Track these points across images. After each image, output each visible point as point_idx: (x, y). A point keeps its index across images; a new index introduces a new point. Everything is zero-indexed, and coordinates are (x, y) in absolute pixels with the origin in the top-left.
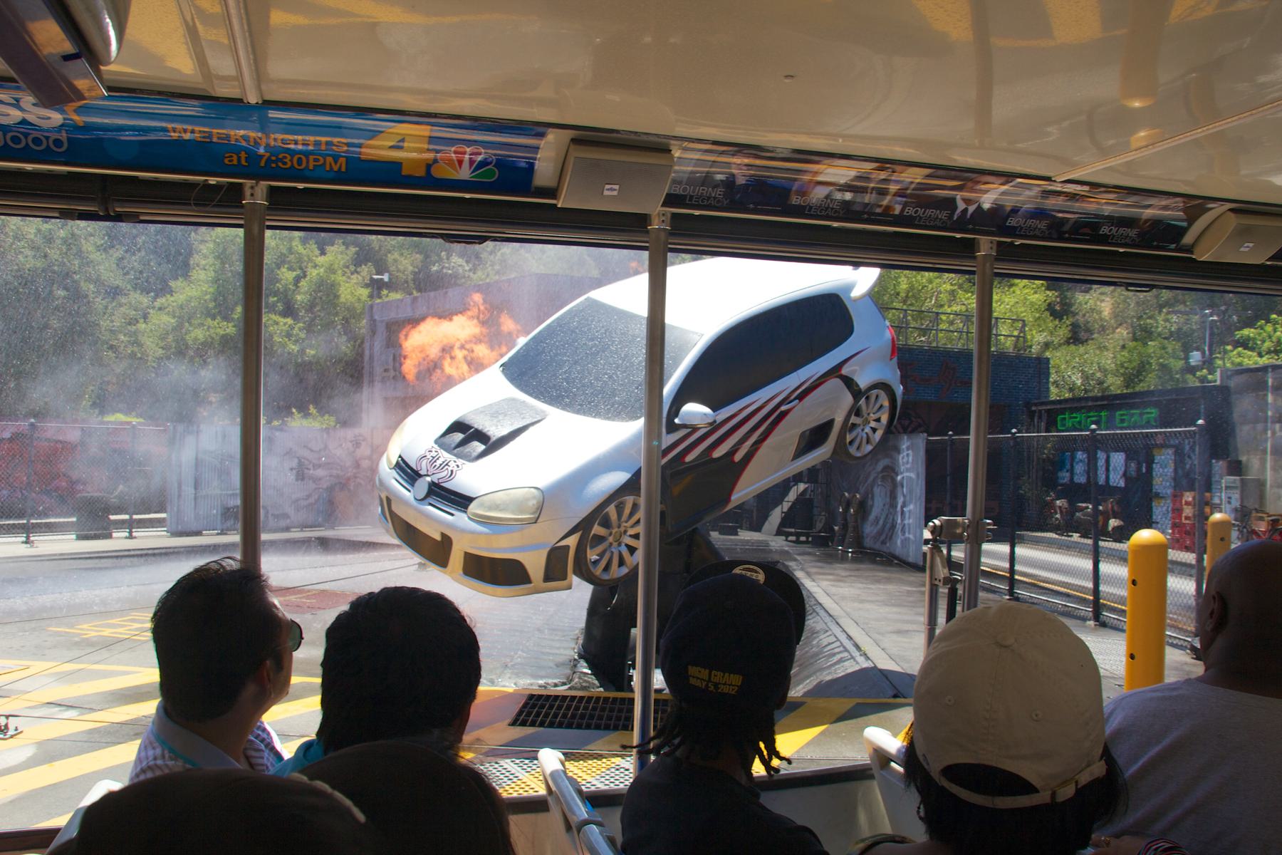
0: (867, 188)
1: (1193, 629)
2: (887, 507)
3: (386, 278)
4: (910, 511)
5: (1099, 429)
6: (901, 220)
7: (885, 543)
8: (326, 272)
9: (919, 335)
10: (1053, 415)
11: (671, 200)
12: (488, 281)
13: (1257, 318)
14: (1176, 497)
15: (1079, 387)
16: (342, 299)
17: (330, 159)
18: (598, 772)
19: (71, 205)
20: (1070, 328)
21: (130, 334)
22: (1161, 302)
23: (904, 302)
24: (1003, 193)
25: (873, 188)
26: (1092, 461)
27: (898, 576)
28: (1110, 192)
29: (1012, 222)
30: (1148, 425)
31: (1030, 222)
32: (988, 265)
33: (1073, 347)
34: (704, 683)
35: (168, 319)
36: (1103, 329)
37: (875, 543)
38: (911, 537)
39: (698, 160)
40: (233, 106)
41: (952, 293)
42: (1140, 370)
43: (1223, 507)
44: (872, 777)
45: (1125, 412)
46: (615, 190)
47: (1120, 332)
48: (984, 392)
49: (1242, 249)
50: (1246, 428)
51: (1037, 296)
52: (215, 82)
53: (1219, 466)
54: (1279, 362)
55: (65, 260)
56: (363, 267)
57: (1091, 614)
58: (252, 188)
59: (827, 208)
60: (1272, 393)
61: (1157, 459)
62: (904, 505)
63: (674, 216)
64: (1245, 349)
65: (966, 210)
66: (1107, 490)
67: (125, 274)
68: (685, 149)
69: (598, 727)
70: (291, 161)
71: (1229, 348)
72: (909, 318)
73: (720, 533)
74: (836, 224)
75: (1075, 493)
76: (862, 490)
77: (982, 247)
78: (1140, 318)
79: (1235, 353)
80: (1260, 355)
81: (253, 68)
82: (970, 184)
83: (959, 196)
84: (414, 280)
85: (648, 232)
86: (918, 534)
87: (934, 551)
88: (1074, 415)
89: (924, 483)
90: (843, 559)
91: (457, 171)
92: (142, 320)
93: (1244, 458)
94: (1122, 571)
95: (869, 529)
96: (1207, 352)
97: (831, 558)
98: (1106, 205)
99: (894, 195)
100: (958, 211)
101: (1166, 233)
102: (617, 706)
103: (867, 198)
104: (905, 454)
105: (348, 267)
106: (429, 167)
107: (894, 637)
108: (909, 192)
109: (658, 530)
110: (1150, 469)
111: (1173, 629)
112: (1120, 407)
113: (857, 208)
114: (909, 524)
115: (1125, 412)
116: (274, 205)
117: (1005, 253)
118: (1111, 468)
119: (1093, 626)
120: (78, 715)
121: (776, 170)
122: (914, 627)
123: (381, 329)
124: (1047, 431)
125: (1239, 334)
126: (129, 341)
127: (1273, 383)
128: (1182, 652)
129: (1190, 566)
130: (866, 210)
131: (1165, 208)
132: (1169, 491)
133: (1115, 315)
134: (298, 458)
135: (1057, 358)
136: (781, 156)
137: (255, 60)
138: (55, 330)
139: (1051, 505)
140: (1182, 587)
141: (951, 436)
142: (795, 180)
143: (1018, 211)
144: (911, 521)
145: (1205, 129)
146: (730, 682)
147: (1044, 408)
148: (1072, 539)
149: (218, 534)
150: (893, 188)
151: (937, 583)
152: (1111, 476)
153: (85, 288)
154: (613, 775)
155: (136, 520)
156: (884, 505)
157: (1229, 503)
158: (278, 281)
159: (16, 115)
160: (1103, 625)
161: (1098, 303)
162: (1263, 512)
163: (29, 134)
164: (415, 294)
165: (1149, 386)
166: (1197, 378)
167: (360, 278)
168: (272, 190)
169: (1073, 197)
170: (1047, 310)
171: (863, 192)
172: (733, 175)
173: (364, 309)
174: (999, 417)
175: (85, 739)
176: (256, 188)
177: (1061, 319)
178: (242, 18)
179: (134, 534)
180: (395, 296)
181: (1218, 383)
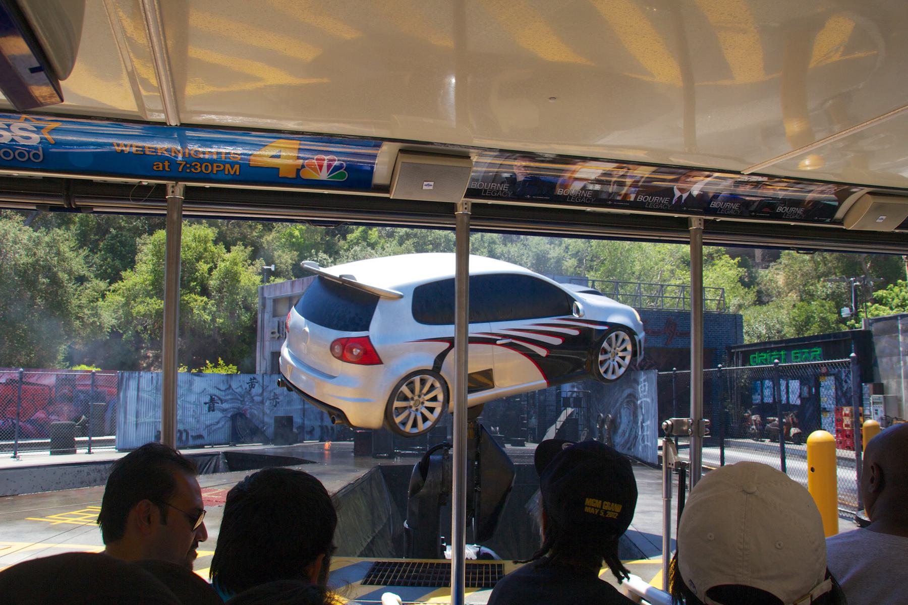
0: (610, 181)
2: (631, 423)
3: (273, 268)
4: (647, 426)
5: (781, 362)
7: (631, 449)
8: (231, 264)
10: (747, 354)
11: (471, 193)
13: (888, 283)
14: (838, 411)
15: (764, 336)
16: (242, 284)
17: (228, 166)
19: (44, 200)
20: (755, 294)
21: (93, 308)
22: (818, 274)
23: (639, 278)
24: (707, 184)
25: (615, 182)
26: (777, 385)
28: (783, 182)
29: (714, 205)
30: (815, 359)
31: (727, 204)
32: (698, 236)
33: (758, 307)
37: (623, 449)
38: (649, 444)
39: (490, 163)
40: (159, 129)
41: (672, 272)
42: (808, 321)
45: (798, 351)
46: (431, 185)
47: (790, 296)
48: (699, 327)
49: (878, 221)
50: (885, 360)
51: (732, 272)
52: (147, 112)
53: (867, 388)
54: (905, 313)
55: (48, 257)
58: (173, 187)
60: (902, 335)
61: (822, 384)
62: (643, 422)
63: (474, 205)
64: (880, 305)
65: (681, 196)
66: (788, 407)
67: (90, 267)
69: (426, 585)
70: (201, 167)
71: (869, 304)
72: (642, 290)
73: (512, 445)
75: (765, 410)
76: (612, 412)
77: (693, 224)
78: (805, 285)
79: (873, 307)
80: (891, 309)
81: (173, 98)
82: (683, 178)
83: (676, 187)
84: (292, 269)
86: (654, 441)
87: (668, 443)
89: (657, 405)
91: (319, 174)
93: (884, 382)
94: (804, 466)
96: (854, 308)
98: (779, 191)
99: (630, 186)
101: (823, 210)
102: (439, 570)
103: (611, 189)
104: (642, 385)
105: (246, 261)
106: (298, 171)
109: (466, 434)
111: (842, 506)
112: (794, 348)
113: (604, 196)
114: (647, 435)
115: (798, 351)
117: (710, 228)
118: (790, 390)
121: (546, 170)
122: (654, 508)
123: (269, 305)
124: (743, 365)
125: (875, 294)
126: (91, 314)
128: (851, 522)
129: (852, 460)
130: (610, 198)
131: (822, 192)
133: (787, 284)
134: (210, 395)
135: (748, 315)
137: (175, 93)
138: (40, 306)
139: (746, 420)
140: (848, 475)
141: (675, 371)
142: (560, 176)
143: (719, 196)
145: (847, 131)
147: (740, 350)
150: (629, 181)
151: (670, 466)
152: (790, 396)
156: (629, 422)
157: (876, 413)
158: (197, 271)
161: (775, 276)
165: (814, 333)
167: (255, 268)
168: (187, 190)
169: (757, 184)
170: (739, 281)
171: (608, 185)
172: (515, 174)
173: (257, 290)
174: (710, 357)
177: (749, 288)
178: (165, 61)
179: (92, 451)
180: (279, 281)
181: (863, 328)
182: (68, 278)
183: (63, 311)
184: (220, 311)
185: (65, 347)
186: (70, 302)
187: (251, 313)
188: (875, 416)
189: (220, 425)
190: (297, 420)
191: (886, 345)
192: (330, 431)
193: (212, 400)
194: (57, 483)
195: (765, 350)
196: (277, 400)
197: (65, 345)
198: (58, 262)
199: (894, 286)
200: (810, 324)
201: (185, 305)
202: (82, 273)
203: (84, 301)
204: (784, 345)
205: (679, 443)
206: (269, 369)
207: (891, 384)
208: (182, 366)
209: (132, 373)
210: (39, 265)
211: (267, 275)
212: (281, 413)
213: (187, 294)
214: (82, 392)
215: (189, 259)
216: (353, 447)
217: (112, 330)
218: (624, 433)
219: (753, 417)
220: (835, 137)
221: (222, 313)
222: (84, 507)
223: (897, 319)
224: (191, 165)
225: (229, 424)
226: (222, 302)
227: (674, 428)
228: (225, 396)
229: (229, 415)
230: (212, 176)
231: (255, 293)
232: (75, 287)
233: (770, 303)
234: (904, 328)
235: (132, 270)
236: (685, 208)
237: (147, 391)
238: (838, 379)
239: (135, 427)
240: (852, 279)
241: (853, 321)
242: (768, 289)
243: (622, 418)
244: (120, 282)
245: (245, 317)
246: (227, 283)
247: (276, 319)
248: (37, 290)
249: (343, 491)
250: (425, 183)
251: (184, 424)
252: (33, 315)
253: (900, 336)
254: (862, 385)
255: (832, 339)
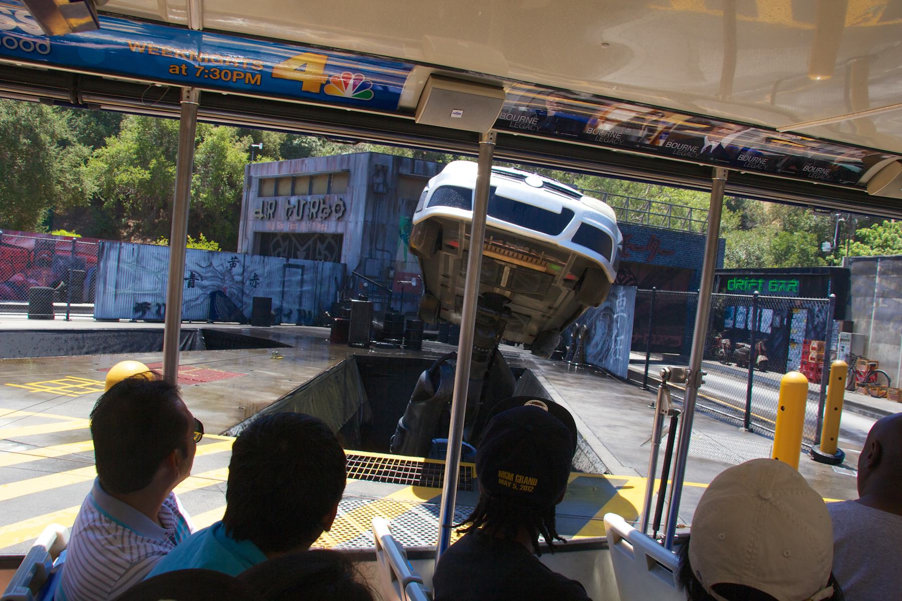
1: (814, 440)
2: (605, 336)
3: (260, 146)
4: (621, 340)
6: (663, 151)
7: (602, 361)
9: (635, 216)
11: (499, 124)
12: (333, 153)
14: (806, 344)
16: (229, 160)
17: (249, 75)
18: (396, 515)
20: (740, 218)
21: (75, 174)
23: (626, 191)
27: (609, 385)
29: (742, 158)
31: (754, 159)
32: (721, 187)
33: (741, 232)
34: (510, 484)
35: (103, 165)
36: (763, 221)
38: (621, 358)
39: (522, 96)
42: (788, 251)
43: (838, 353)
44: (607, 548)
45: (776, 282)
50: (858, 299)
53: (838, 324)
56: (245, 137)
57: (743, 423)
58: (188, 92)
59: (611, 138)
60: (879, 276)
62: (617, 336)
63: (498, 134)
64: (861, 243)
68: (514, 88)
70: (220, 74)
74: (615, 150)
75: (737, 335)
76: (588, 322)
77: (717, 174)
80: (872, 248)
85: (479, 145)
88: (740, 281)
90: (572, 370)
91: (343, 91)
92: (83, 164)
93: (855, 320)
94: (774, 396)
95: (591, 350)
96: (835, 243)
97: (562, 369)
100: (705, 147)
104: (621, 300)
105: (234, 137)
106: (322, 86)
107: (606, 429)
108: (671, 130)
110: (789, 323)
112: (772, 277)
115: (776, 282)
116: (204, 105)
117: (733, 179)
118: (762, 319)
119: (744, 431)
120: (27, 450)
125: (859, 231)
127: (880, 270)
128: (805, 454)
129: (815, 393)
130: (639, 141)
132: (802, 339)
136: (583, 98)
138: (20, 167)
139: (717, 342)
142: (591, 116)
144: (621, 347)
146: (529, 483)
147: (719, 274)
148: (730, 367)
149: (130, 322)
150: (660, 128)
151: (663, 413)
152: (762, 325)
153: (43, 138)
154: (406, 518)
155: (66, 302)
156: (603, 334)
157: (842, 350)
159: (11, 24)
160: (751, 431)
162: (865, 359)
163: (21, 39)
164: (281, 160)
165: (792, 264)
166: (827, 261)
167: (242, 145)
168: (203, 94)
171: (638, 129)
175: (31, 468)
176: (191, 92)
177: (734, 211)
179: (70, 318)
180: (267, 160)
181: (842, 266)
182: (50, 140)
183: (44, 174)
184: (204, 186)
185: (45, 211)
186: (52, 166)
187: (236, 190)
188: (841, 352)
189: (199, 302)
190: (276, 302)
191: (862, 285)
192: (307, 315)
193: (192, 276)
194: (35, 348)
195: (743, 277)
196: (257, 281)
197: (45, 209)
198: (40, 123)
199: (879, 226)
200: (789, 254)
201: (169, 177)
202: (65, 137)
203: (66, 165)
204: (763, 274)
205: (651, 359)
206: (250, 249)
207: (861, 323)
208: (163, 239)
209: (113, 243)
210: (21, 124)
211: (253, 153)
212: (260, 294)
213: (171, 166)
214: (61, 258)
215: (176, 130)
216: (330, 333)
217: (94, 197)
218: (597, 345)
219: (724, 341)
220: (886, 109)
221: (206, 188)
222: (62, 376)
223: (877, 261)
224: (209, 71)
225: (208, 301)
226: (207, 177)
227: (671, 377)
228: (206, 273)
229: (208, 293)
230: (231, 84)
231: (241, 171)
232: (57, 150)
233: (753, 229)
234: (882, 270)
235: (116, 137)
236: (712, 159)
237: (127, 263)
238: (810, 312)
239: (114, 296)
240: (838, 214)
241: (832, 257)
242: (753, 215)
243: (597, 329)
244: (103, 148)
245: (229, 194)
246: (213, 157)
247: (261, 199)
248: (17, 150)
249: (318, 379)
250: (454, 111)
251: (163, 298)
252: (13, 176)
253: (877, 277)
254: (833, 322)
255: (811, 274)
